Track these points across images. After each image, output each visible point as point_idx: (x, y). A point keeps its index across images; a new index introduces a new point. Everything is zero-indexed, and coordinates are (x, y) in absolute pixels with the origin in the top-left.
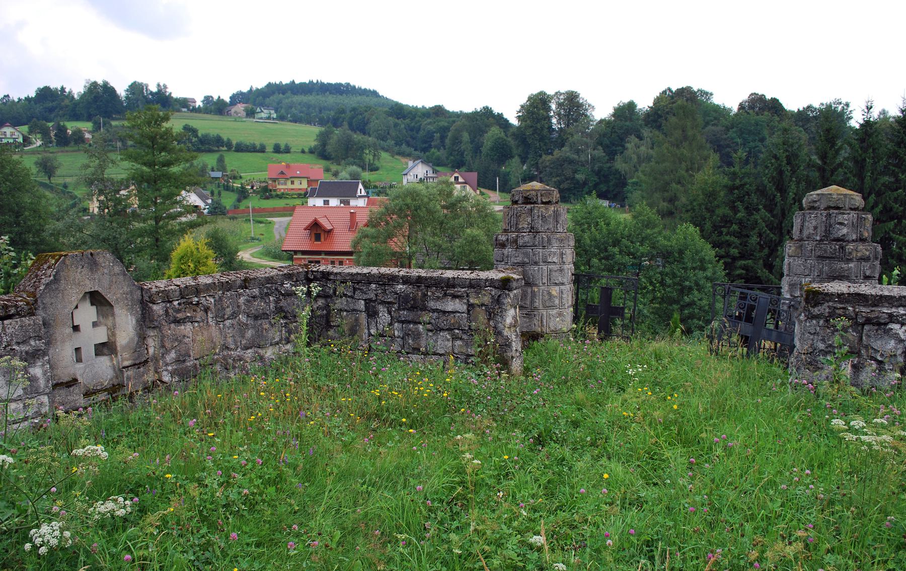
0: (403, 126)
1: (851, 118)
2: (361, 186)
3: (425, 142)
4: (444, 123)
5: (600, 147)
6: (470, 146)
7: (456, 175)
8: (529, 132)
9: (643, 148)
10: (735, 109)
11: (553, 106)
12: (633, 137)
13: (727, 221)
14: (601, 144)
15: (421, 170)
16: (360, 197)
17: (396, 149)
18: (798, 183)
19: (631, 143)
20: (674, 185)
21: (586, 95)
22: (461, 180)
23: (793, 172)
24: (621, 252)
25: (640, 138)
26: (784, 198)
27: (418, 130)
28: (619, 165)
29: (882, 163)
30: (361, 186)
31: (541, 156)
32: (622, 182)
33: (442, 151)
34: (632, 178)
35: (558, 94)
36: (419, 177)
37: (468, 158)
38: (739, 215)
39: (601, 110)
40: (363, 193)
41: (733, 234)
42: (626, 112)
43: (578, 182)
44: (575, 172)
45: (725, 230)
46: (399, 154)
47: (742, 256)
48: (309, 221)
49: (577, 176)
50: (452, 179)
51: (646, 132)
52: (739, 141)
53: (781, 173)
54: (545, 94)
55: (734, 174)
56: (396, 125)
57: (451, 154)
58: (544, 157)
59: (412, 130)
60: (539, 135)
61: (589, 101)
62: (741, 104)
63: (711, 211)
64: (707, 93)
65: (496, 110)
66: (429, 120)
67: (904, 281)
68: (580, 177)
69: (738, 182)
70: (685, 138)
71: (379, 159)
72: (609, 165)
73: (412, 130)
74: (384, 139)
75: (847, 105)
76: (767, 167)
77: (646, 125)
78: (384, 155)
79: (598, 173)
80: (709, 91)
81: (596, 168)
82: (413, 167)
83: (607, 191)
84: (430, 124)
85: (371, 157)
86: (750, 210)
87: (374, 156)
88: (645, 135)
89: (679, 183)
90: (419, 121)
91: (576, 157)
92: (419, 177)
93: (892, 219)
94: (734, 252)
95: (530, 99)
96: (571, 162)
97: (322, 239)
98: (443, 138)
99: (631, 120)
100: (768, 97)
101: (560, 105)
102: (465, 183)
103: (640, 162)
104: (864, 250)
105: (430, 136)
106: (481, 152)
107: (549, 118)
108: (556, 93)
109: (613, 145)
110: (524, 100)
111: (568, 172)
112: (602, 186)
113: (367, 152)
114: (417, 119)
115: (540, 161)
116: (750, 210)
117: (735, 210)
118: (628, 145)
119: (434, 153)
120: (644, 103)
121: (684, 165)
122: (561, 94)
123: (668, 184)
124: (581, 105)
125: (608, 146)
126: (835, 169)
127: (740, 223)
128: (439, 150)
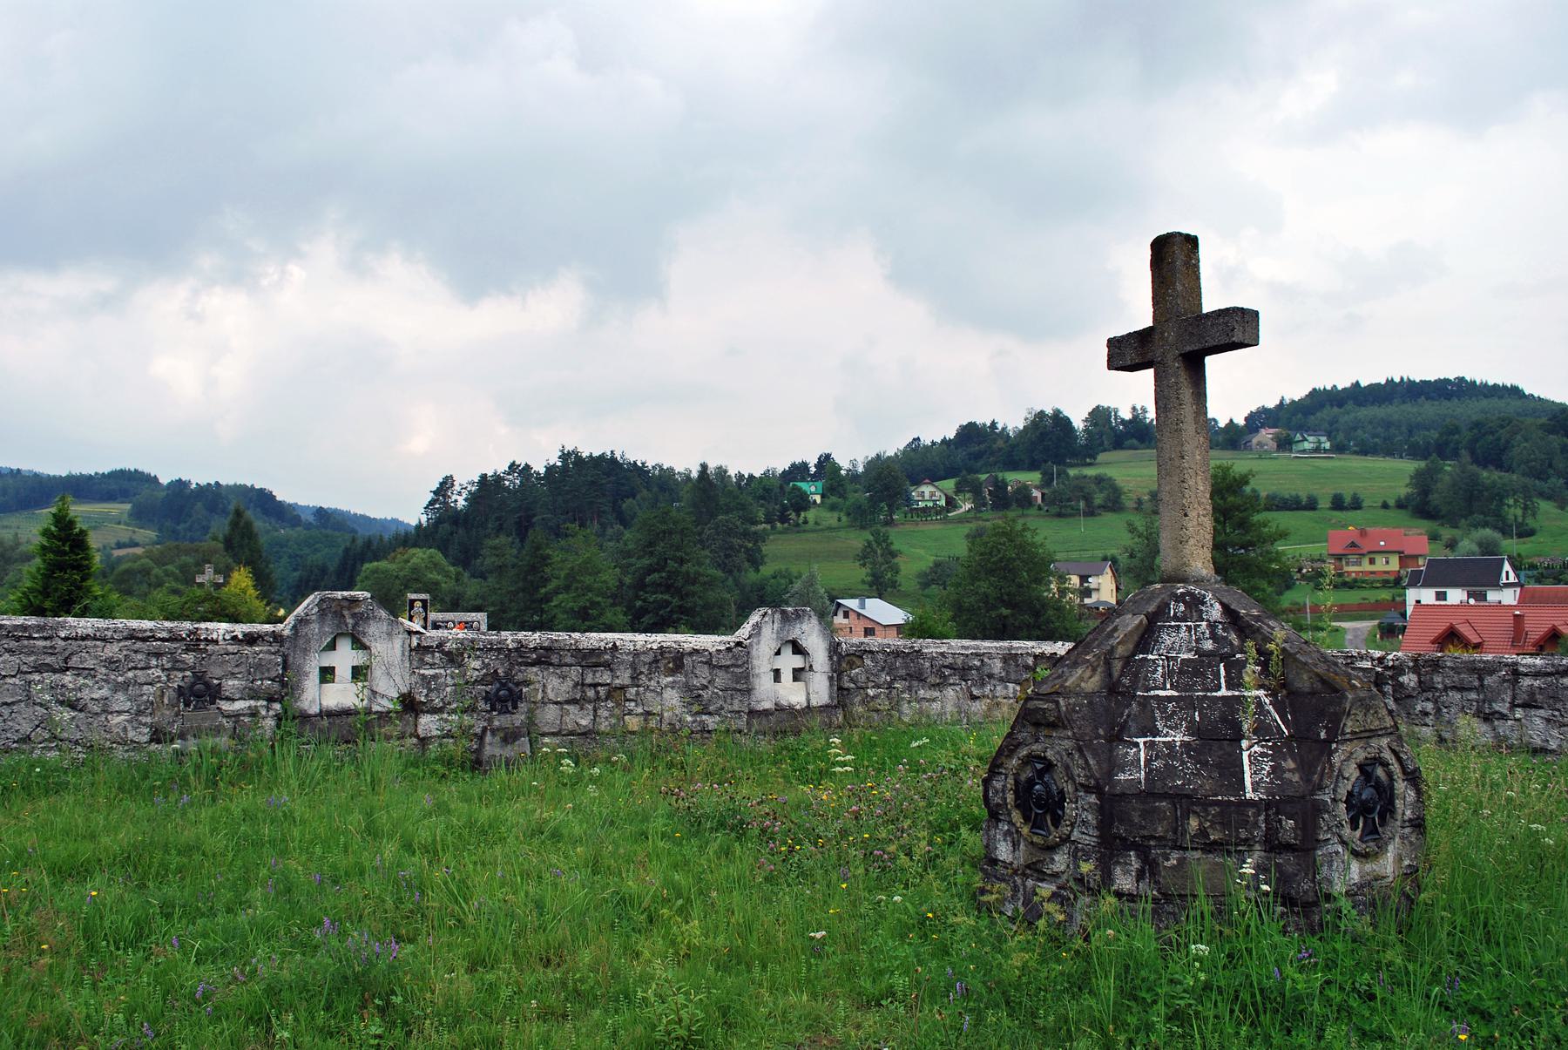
2: (1507, 567)
21: (1067, 412)
30: (1507, 567)
40: (1512, 578)
48: (1440, 628)
71: (1534, 515)
78: (1545, 506)
85: (1519, 512)
87: (1525, 508)
113: (1511, 502)
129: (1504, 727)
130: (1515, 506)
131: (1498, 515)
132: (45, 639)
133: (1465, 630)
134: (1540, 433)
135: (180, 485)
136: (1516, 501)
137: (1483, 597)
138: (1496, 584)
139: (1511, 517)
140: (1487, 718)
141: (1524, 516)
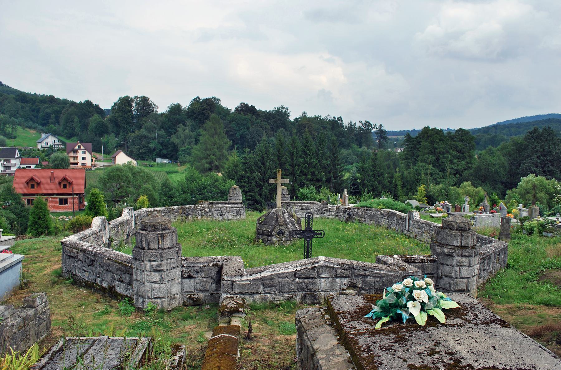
0: (28, 108)
1: (289, 116)
2: (17, 151)
3: (45, 120)
4: (56, 108)
5: (162, 130)
6: (79, 125)
7: (79, 145)
8: (120, 119)
9: (187, 131)
10: (233, 110)
11: (134, 105)
12: (181, 124)
13: (243, 177)
14: (163, 128)
15: (51, 140)
16: (18, 158)
17: (26, 124)
18: (270, 161)
19: (181, 127)
20: (212, 156)
21: (153, 99)
22: (82, 148)
23: (268, 157)
24: (207, 192)
25: (185, 125)
26: (265, 168)
27: (38, 111)
28: (174, 139)
29: (300, 153)
30: (17, 151)
31: (127, 133)
32: (175, 149)
33: (57, 126)
34: (181, 147)
35: (137, 97)
36: (49, 144)
37: (77, 130)
38: (248, 174)
39: (162, 107)
40: (19, 155)
41: (245, 182)
42: (176, 109)
43: (150, 149)
44: (149, 143)
45: (242, 181)
46: (27, 127)
47: (249, 191)
48: (27, 178)
49: (150, 146)
50: (77, 147)
51: (189, 122)
52: (237, 128)
53: (263, 157)
54: (129, 97)
55: (245, 157)
56: (23, 108)
57: (66, 129)
58: (129, 134)
59: (33, 111)
60: (126, 121)
61: (155, 103)
62: (236, 108)
63: (236, 173)
64: (217, 99)
65: (94, 103)
66: (46, 106)
67: (560, 180)
68: (152, 146)
69: (247, 161)
70: (216, 133)
71: (16, 131)
72: (168, 139)
73: (33, 111)
74: (15, 116)
75: (287, 109)
76: (257, 155)
77: (188, 118)
78: (19, 128)
79: (162, 144)
80: (219, 98)
81: (161, 141)
82: (45, 139)
83: (167, 154)
84: (47, 108)
85: (10, 130)
86: (252, 172)
87: (13, 128)
88: (188, 124)
89: (214, 155)
90: (38, 105)
91: (149, 134)
92: (49, 144)
93: (304, 175)
94: (247, 189)
95: (120, 99)
96: (145, 137)
97: (36, 187)
98: (57, 118)
99: (179, 114)
100: (250, 105)
101: (137, 104)
102: (85, 149)
103: (186, 138)
104: (287, 196)
105: (48, 116)
106: (87, 129)
107: (131, 111)
108: (135, 97)
109: (170, 128)
110: (116, 100)
111: (144, 143)
112: (163, 151)
113: (8, 126)
114: (37, 104)
115: (127, 136)
116: (252, 172)
117: (246, 172)
118: (178, 129)
119: (52, 128)
120: (185, 104)
121: (216, 146)
122: (138, 98)
123: (209, 155)
124: (150, 105)
125: (166, 129)
126: (283, 156)
127: (248, 177)
128: (55, 125)
129: (224, 217)
130: (9, 128)
131: (3, 131)
132: (183, 337)
133: (35, 177)
134: (14, 101)
135: (246, 110)
136: (10, 126)
137: (9, 162)
138: (14, 157)
139: (7, 131)
140: (221, 215)
141: (12, 131)
